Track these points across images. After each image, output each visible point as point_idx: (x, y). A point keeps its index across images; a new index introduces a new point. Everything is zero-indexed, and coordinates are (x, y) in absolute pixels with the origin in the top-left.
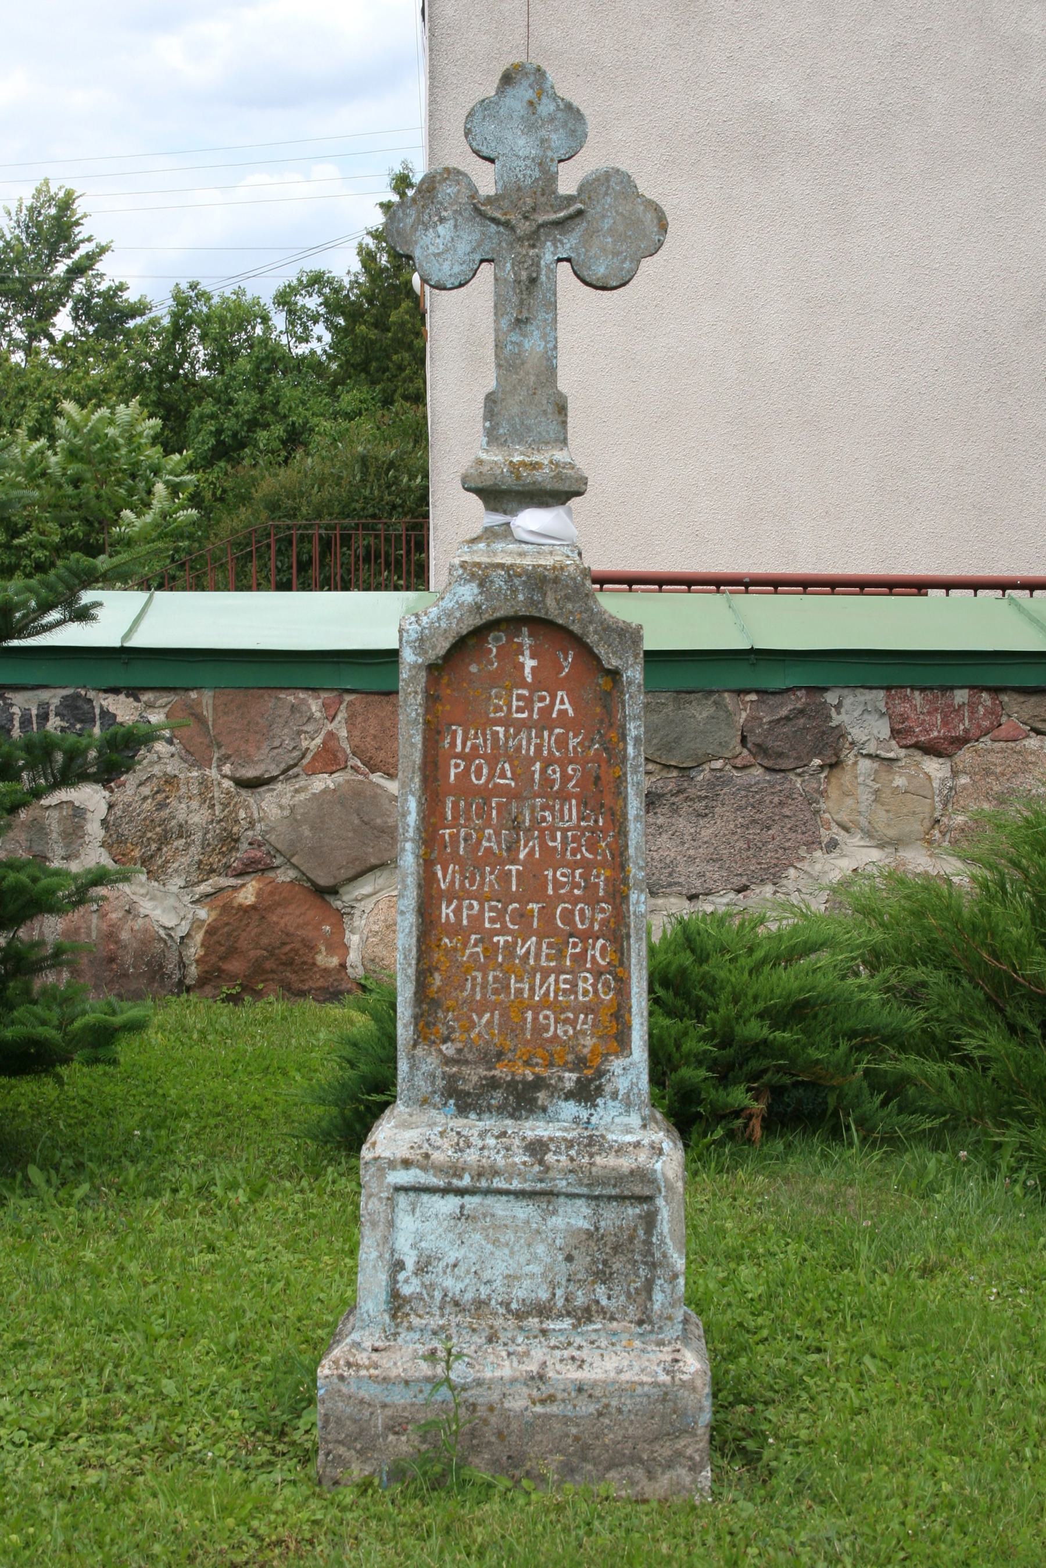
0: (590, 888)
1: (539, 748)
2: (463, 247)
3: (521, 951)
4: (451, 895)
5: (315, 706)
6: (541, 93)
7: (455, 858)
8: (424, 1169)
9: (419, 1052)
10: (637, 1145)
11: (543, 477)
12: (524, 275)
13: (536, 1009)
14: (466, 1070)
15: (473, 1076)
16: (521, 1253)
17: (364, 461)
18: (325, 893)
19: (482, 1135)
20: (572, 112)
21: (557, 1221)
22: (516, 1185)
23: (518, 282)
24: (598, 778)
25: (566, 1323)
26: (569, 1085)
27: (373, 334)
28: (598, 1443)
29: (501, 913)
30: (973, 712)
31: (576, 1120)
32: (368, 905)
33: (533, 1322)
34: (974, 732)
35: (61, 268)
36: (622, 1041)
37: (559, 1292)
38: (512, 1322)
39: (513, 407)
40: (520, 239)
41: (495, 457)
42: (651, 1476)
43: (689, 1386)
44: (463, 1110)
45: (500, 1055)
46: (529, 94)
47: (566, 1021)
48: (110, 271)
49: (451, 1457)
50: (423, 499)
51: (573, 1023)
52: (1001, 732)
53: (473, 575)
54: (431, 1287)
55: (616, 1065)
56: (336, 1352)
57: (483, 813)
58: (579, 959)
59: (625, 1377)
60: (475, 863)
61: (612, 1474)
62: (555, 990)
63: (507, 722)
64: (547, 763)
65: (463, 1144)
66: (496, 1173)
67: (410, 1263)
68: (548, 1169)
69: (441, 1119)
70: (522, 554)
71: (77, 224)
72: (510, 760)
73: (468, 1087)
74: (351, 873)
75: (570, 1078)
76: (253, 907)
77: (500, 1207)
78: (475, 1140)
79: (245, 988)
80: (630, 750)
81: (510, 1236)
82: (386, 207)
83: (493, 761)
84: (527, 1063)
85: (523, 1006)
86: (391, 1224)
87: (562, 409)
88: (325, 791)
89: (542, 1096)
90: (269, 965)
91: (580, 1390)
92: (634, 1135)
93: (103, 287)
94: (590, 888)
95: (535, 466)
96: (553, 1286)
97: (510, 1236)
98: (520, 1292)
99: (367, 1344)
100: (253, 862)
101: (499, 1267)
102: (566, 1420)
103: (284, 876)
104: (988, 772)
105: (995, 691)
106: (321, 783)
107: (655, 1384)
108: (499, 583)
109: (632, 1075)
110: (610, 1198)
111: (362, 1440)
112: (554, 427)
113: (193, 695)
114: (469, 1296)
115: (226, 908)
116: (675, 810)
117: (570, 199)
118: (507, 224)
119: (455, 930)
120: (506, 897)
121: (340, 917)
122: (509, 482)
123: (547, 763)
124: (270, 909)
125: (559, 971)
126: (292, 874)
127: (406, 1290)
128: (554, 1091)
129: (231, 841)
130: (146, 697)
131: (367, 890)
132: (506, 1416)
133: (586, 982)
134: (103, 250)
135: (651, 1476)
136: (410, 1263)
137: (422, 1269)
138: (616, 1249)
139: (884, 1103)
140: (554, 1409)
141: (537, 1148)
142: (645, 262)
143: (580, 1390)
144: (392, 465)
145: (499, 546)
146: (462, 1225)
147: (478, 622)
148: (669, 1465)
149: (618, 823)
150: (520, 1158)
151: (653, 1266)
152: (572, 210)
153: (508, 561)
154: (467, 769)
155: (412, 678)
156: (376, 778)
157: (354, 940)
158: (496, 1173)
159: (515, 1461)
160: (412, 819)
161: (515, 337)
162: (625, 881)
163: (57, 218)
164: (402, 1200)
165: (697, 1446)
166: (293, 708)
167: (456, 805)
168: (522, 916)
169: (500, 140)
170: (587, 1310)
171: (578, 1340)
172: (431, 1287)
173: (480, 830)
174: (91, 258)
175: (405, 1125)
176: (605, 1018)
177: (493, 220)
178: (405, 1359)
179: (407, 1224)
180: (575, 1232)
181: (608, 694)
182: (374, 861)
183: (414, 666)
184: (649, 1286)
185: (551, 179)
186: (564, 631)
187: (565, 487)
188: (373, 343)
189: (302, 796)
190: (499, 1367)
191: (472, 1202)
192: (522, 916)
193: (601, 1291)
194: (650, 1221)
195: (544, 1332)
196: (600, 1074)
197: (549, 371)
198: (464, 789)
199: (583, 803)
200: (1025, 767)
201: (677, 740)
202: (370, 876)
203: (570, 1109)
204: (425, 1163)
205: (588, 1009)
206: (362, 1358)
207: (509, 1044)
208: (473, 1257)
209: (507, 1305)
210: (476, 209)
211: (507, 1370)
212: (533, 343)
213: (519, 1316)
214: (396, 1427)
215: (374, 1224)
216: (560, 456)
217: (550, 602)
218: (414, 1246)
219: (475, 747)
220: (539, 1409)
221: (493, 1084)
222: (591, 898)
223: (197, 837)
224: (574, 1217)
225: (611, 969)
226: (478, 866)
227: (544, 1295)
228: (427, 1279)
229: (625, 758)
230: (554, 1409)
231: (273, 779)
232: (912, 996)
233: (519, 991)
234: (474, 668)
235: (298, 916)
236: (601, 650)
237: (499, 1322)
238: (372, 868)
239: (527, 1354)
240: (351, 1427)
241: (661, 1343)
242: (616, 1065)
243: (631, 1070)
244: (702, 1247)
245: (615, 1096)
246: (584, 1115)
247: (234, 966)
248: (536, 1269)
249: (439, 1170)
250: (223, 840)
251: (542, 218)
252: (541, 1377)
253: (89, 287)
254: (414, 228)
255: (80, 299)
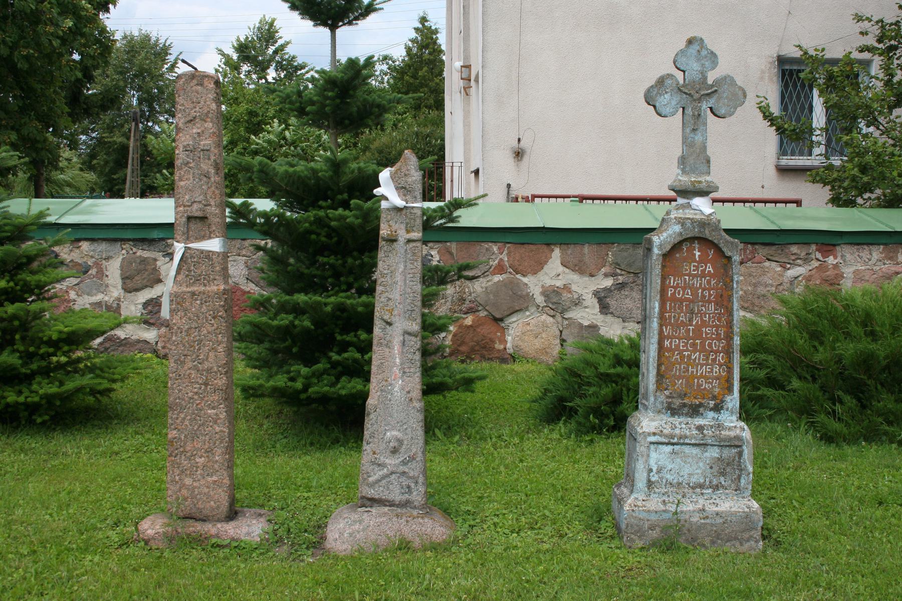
0: (718, 335)
1: (701, 284)
2: (674, 103)
3: (693, 358)
4: (668, 337)
5: (495, 249)
6: (702, 47)
7: (670, 324)
8: (661, 436)
9: (658, 394)
10: (735, 427)
11: (703, 186)
12: (696, 113)
13: (698, 378)
14: (674, 400)
15: (677, 402)
16: (694, 466)
17: (417, 134)
18: (498, 320)
19: (680, 423)
20: (713, 55)
21: (707, 454)
22: (693, 441)
23: (693, 115)
24: (722, 296)
25: (710, 491)
26: (711, 406)
27: (411, 81)
28: (723, 533)
29: (686, 344)
30: (745, 252)
31: (713, 418)
32: (514, 325)
33: (698, 490)
34: (745, 260)
35: (271, 50)
36: (730, 390)
37: (707, 480)
38: (691, 490)
39: (691, 160)
40: (695, 100)
41: (684, 178)
42: (741, 544)
43: (755, 513)
44: (673, 415)
45: (685, 395)
46: (698, 48)
47: (709, 383)
48: (290, 50)
49: (673, 539)
50: (442, 148)
51: (712, 383)
52: (755, 260)
53: (679, 222)
54: (661, 478)
55: (728, 398)
56: (629, 501)
57: (680, 308)
58: (714, 360)
59: (733, 509)
60: (677, 326)
61: (728, 544)
62: (705, 371)
63: (689, 275)
64: (704, 290)
65: (674, 427)
66: (686, 437)
67: (655, 469)
68: (705, 436)
69: (665, 418)
70: (695, 214)
71: (277, 32)
72: (690, 289)
73: (675, 407)
74: (509, 313)
75: (712, 403)
76: (471, 326)
77: (687, 449)
78: (677, 425)
79: (467, 357)
80: (735, 286)
81: (690, 460)
82: (417, 29)
83: (684, 289)
84: (695, 398)
85: (694, 377)
86: (648, 456)
87: (708, 162)
88: (499, 281)
89: (701, 410)
90: (477, 348)
91: (717, 514)
92: (731, 423)
93: (287, 57)
94: (718, 335)
95: (700, 182)
96: (705, 477)
97: (690, 460)
98: (694, 480)
99: (640, 498)
100: (471, 308)
101: (686, 471)
102: (712, 525)
103: (483, 314)
104: (750, 275)
105: (753, 244)
106: (497, 278)
107: (744, 512)
108: (688, 225)
109: (733, 402)
110: (726, 446)
111: (640, 533)
112: (706, 168)
113: (448, 244)
114: (675, 481)
115: (461, 326)
116: (632, 289)
117: (712, 86)
118: (690, 95)
119: (670, 350)
120: (688, 338)
121: (503, 330)
122: (691, 188)
123: (704, 290)
124: (478, 326)
125: (707, 365)
126: (486, 313)
127: (653, 479)
128: (706, 408)
129: (462, 300)
130: (430, 245)
131: (514, 319)
132: (691, 523)
133: (716, 369)
134: (288, 43)
135: (741, 544)
136: (655, 469)
137: (659, 472)
138: (728, 464)
139: (754, 405)
140: (708, 521)
141: (700, 428)
142: (739, 109)
143: (717, 514)
144: (428, 136)
145: (687, 211)
146: (673, 456)
147: (681, 239)
148: (748, 540)
149: (730, 313)
150: (695, 432)
151: (741, 470)
152: (713, 89)
153: (691, 216)
154: (675, 292)
155: (657, 259)
156: (518, 276)
157: (509, 338)
158: (686, 437)
159: (694, 539)
160: (657, 310)
161: (692, 135)
162: (732, 332)
163: (268, 30)
164: (652, 447)
165: (757, 534)
166: (487, 249)
167: (670, 305)
168: (694, 345)
169: (687, 64)
170: (717, 486)
171: (714, 497)
172: (661, 478)
173: (679, 314)
174: (283, 47)
175: (652, 420)
176: (723, 381)
177: (685, 93)
178: (655, 503)
179: (654, 455)
180: (713, 458)
181: (726, 265)
182: (517, 308)
183: (658, 255)
184: (739, 477)
185: (705, 78)
186: (712, 242)
187: (709, 190)
188: (411, 84)
189: (490, 283)
190: (688, 507)
191: (677, 448)
192: (694, 345)
193: (722, 479)
194: (740, 454)
195: (702, 494)
196: (722, 401)
197: (704, 148)
198: (674, 299)
199: (716, 304)
200: (764, 273)
201: (634, 262)
202: (515, 314)
203: (711, 414)
204: (661, 434)
205: (717, 378)
206: (639, 503)
207: (689, 391)
208: (677, 467)
209: (689, 484)
210: (679, 89)
211: (691, 507)
212: (698, 138)
213: (693, 488)
214: (652, 528)
215: (642, 456)
216: (708, 178)
217: (707, 232)
218: (656, 463)
219: (678, 284)
220: (702, 521)
221: (684, 405)
222: (719, 339)
223: (450, 299)
224: (713, 453)
225: (725, 364)
226: (678, 327)
227: (702, 481)
228: (661, 475)
229: (732, 288)
230: (708, 521)
231: (479, 277)
232: (761, 365)
233: (693, 372)
234: (678, 255)
235: (487, 330)
236: (725, 250)
237: (686, 490)
238: (517, 311)
239: (697, 501)
240: (636, 528)
241: (743, 497)
242: (728, 398)
243: (733, 400)
244: (760, 462)
245: (727, 409)
246: (716, 416)
247: (463, 348)
248: (699, 471)
249: (666, 436)
250: (459, 300)
251: (702, 93)
252: (704, 510)
253: (281, 58)
254: (656, 95)
255: (278, 62)
